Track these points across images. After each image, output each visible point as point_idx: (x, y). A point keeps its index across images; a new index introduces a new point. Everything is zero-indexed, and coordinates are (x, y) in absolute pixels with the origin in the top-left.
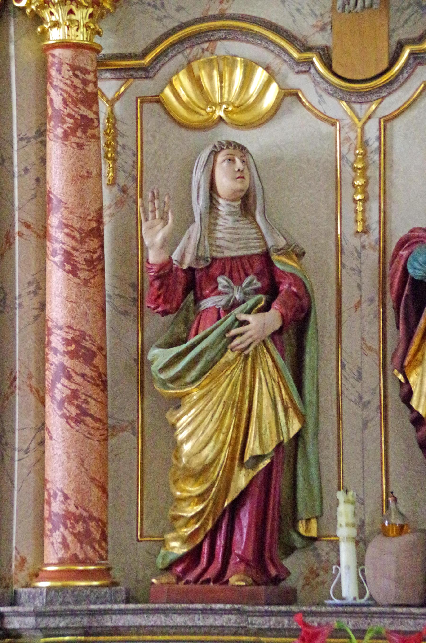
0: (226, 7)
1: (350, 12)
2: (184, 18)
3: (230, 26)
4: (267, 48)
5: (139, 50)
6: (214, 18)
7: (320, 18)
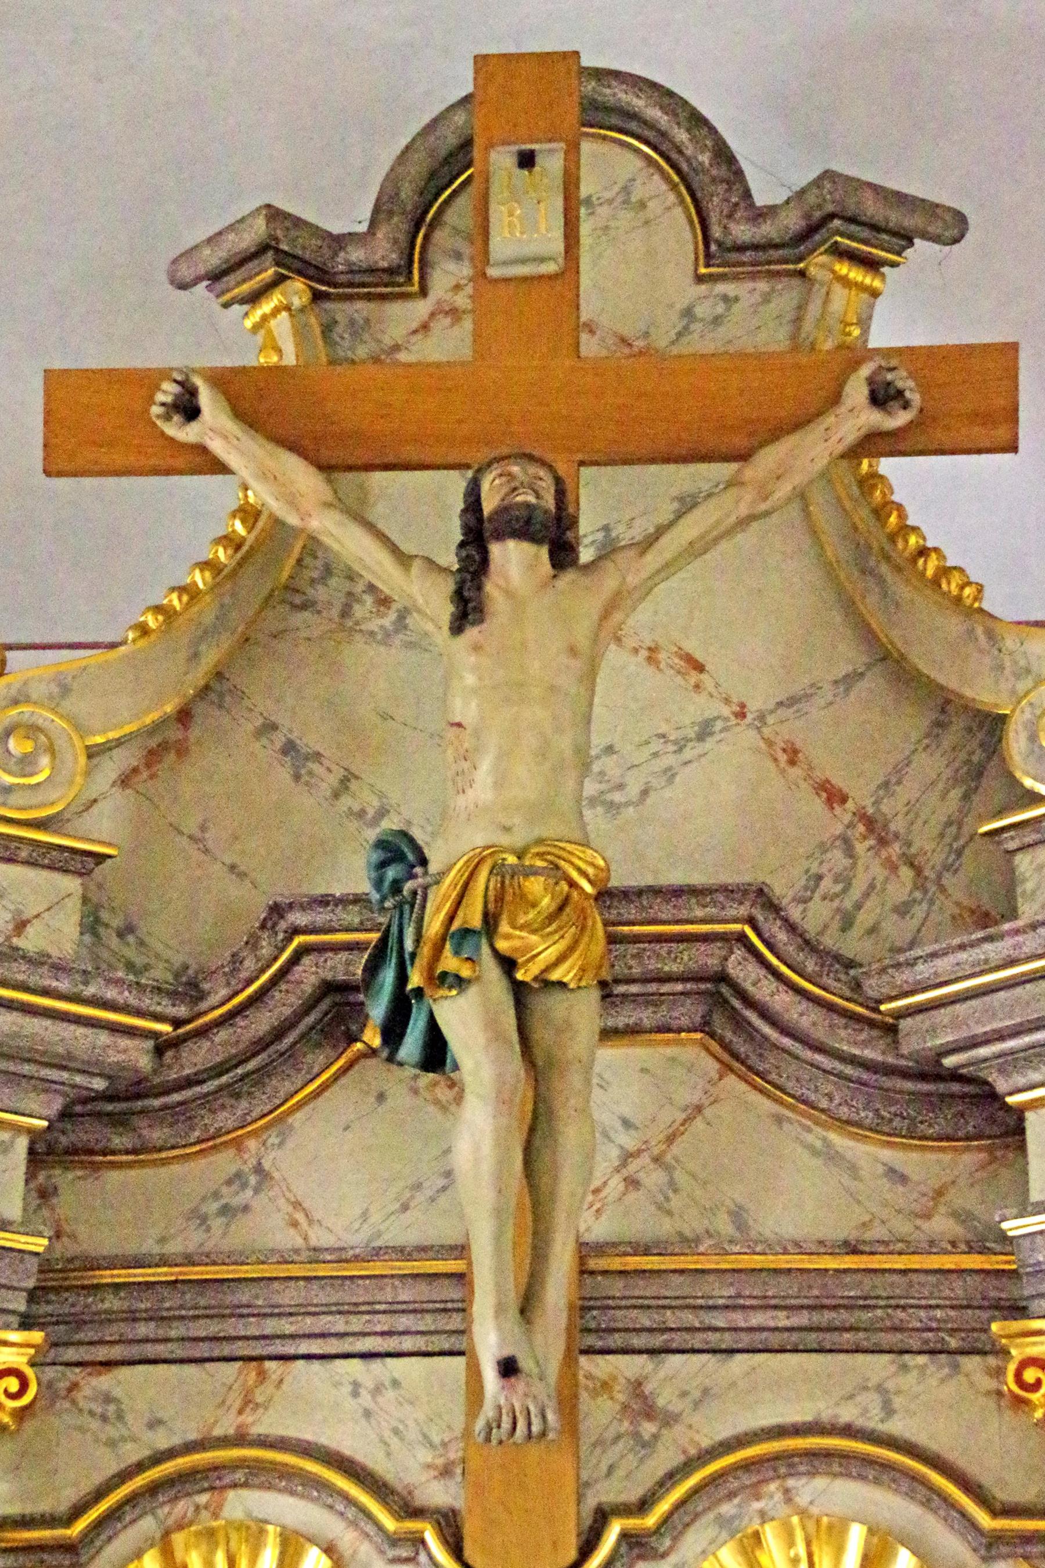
0: (250, 1419)
1: (501, 1442)
2: (162, 1441)
3: (257, 1460)
4: (331, 1507)
5: (63, 1507)
6: (224, 1442)
7: (441, 1451)
